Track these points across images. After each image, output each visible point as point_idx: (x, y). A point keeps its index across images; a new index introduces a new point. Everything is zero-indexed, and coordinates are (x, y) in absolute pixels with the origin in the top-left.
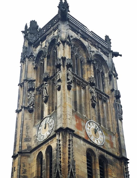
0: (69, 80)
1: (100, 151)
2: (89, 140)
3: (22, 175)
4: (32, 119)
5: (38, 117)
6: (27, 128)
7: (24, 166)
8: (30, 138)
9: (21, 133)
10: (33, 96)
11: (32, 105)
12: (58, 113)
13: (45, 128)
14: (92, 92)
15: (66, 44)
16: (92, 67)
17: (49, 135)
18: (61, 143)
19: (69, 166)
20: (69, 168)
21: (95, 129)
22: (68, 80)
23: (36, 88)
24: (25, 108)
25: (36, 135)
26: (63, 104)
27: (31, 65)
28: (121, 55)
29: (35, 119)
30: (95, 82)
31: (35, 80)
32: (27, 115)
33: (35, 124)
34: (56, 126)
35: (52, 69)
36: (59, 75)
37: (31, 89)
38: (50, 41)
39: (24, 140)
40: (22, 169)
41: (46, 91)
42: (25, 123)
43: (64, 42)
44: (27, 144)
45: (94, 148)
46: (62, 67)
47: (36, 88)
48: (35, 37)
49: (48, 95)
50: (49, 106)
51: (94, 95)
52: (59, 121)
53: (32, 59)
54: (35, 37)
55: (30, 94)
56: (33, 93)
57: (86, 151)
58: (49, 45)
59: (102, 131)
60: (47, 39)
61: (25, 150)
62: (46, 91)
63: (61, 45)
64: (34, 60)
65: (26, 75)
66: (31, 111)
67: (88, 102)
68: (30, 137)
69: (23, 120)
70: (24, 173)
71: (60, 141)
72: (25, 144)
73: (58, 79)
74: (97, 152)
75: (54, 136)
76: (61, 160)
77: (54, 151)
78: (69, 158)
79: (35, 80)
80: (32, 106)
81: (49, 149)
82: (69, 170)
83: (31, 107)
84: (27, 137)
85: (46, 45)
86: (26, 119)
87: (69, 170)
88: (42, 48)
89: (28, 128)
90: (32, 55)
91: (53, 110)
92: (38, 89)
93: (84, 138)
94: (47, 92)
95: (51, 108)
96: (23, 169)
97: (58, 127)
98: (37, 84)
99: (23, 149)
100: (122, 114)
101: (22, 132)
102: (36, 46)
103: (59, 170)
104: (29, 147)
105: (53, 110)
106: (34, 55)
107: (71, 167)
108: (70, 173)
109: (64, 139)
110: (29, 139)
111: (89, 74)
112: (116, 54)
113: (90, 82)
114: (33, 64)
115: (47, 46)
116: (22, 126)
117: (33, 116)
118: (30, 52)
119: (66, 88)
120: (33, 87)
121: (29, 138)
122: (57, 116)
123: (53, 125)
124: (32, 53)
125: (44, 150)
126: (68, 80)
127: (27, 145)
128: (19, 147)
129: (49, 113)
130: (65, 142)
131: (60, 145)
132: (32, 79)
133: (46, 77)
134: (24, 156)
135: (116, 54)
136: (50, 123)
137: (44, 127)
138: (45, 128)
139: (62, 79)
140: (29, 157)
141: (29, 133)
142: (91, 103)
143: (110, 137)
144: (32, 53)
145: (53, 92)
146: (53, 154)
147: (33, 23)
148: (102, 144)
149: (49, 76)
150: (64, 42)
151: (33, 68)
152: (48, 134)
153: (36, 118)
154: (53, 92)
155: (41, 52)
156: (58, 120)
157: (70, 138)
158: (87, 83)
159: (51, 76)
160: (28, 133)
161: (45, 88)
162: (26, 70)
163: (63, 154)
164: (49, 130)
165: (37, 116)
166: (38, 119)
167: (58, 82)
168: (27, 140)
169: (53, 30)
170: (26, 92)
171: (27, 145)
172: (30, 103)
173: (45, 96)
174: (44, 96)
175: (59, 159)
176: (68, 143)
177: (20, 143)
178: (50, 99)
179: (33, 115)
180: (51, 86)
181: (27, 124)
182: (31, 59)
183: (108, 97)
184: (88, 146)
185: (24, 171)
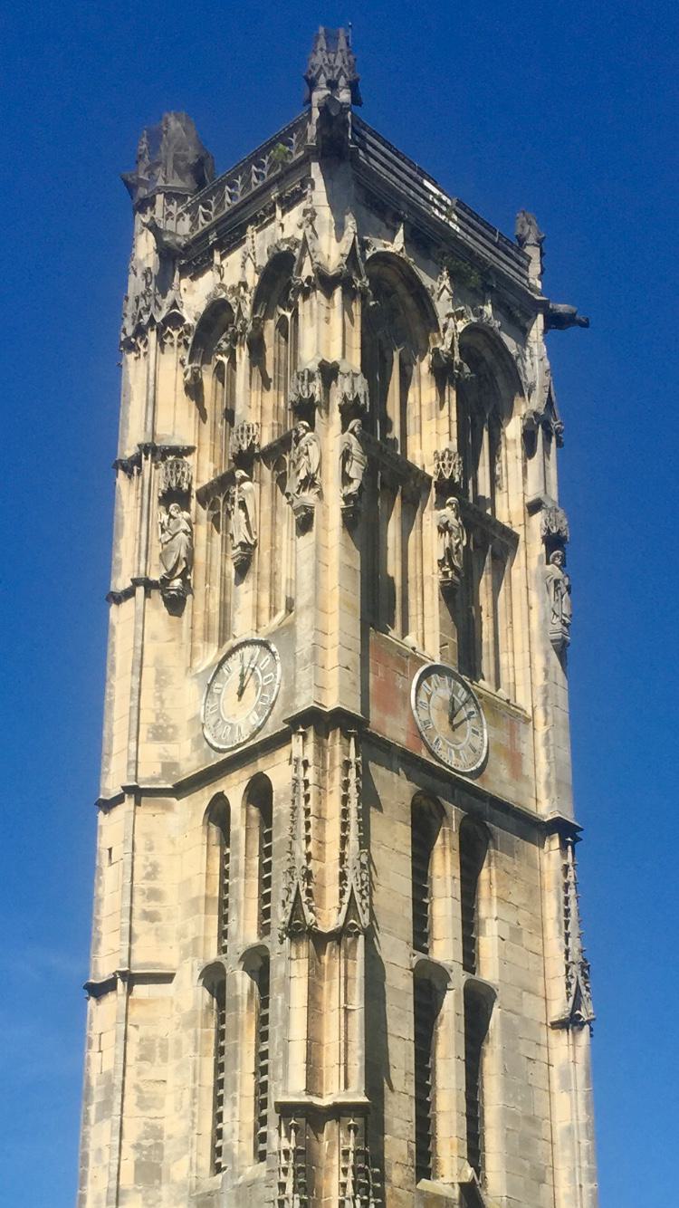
0: (351, 480)
2: (424, 754)
4: (181, 636)
5: (207, 629)
6: (162, 680)
7: (151, 849)
8: (173, 727)
9: (136, 702)
10: (185, 532)
12: (298, 638)
13: (240, 694)
17: (259, 729)
18: (311, 775)
21: (452, 701)
23: (195, 487)
24: (149, 585)
29: (192, 636)
31: (189, 451)
33: (196, 664)
34: (291, 694)
35: (269, 406)
36: (307, 454)
38: (263, 261)
39: (149, 732)
41: (247, 516)
42: (148, 660)
43: (326, 282)
44: (162, 751)
47: (195, 487)
48: (187, 217)
49: (255, 537)
52: (304, 677)
53: (176, 334)
54: (187, 217)
55: (171, 517)
56: (186, 514)
57: (409, 803)
58: (261, 281)
59: (478, 708)
60: (249, 241)
61: (154, 780)
62: (247, 516)
64: (185, 342)
65: (150, 418)
67: (427, 572)
68: (172, 722)
69: (139, 643)
70: (149, 876)
71: (306, 764)
73: (302, 475)
75: (280, 740)
76: (311, 804)
77: (283, 800)
79: (189, 451)
80: (178, 577)
81: (260, 793)
82: (342, 893)
84: (161, 721)
85: (243, 275)
86: (154, 638)
88: (222, 286)
89: (165, 681)
90: (175, 319)
91: (273, 611)
92: (206, 497)
93: (404, 751)
94: (248, 524)
96: (147, 859)
97: (303, 703)
98: (202, 470)
99: (144, 773)
101: (139, 695)
102: (195, 271)
103: (303, 894)
105: (273, 611)
106: (185, 315)
108: (345, 908)
109: (324, 760)
110: (170, 730)
113: (441, 475)
114: (182, 362)
115: (251, 285)
116: (138, 669)
117: (185, 625)
120: (185, 486)
121: (168, 726)
122: (298, 649)
123: (277, 686)
124: (174, 305)
125: (234, 788)
127: (160, 756)
128: (129, 763)
129: (258, 625)
130: (322, 772)
131: (306, 783)
132: (176, 442)
133: (245, 447)
137: (236, 689)
138: (240, 694)
141: (167, 704)
143: (512, 734)
144: (174, 305)
145: (274, 524)
146: (274, 815)
147: (381, 810)
148: (473, 764)
149: (259, 445)
150: (326, 282)
151: (181, 387)
152: (256, 720)
153: (199, 634)
154: (274, 524)
155: (218, 313)
156: (300, 672)
157: (348, 755)
159: (266, 440)
160: (162, 702)
161: (243, 505)
162: (151, 394)
163: (318, 823)
164: (257, 707)
165: (199, 624)
166: (207, 638)
167: (304, 490)
169: (279, 199)
170: (155, 501)
171: (160, 756)
172: (170, 567)
173: (241, 544)
174: (236, 542)
175: (304, 842)
177: (133, 744)
178: (262, 557)
180: (332, 999)
181: (158, 661)
182: (172, 336)
185: (149, 869)
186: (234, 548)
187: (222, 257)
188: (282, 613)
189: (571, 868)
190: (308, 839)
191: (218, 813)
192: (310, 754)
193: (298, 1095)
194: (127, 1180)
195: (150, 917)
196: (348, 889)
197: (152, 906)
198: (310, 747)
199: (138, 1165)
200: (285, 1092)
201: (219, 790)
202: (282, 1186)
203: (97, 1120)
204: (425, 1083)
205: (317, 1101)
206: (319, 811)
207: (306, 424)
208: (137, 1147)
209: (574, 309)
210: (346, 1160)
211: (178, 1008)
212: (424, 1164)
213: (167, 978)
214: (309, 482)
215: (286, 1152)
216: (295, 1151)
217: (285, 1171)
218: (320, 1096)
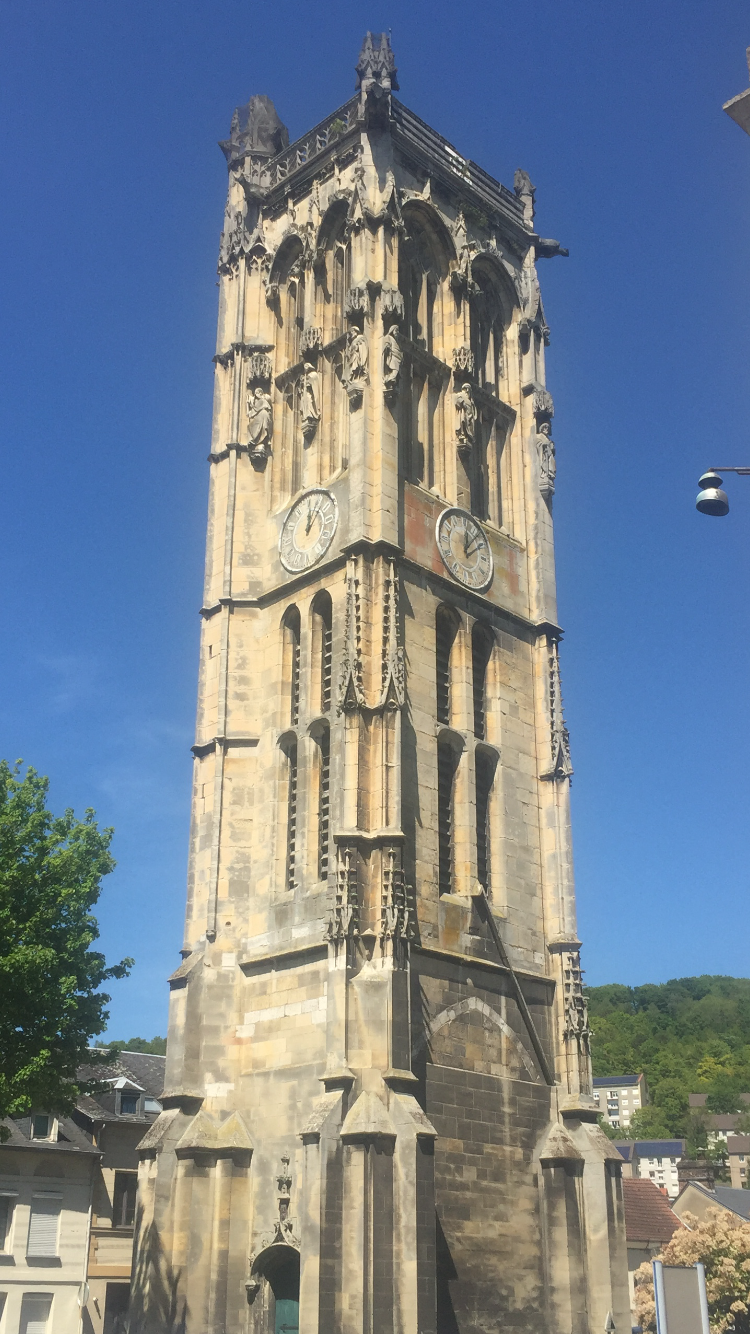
10: (267, 409)
18: (361, 591)
24: (240, 449)
25: (276, 547)
31: (270, 349)
41: (313, 398)
81: (322, 604)
82: (384, 679)
130: (369, 589)
186: (303, 421)
190: (358, 639)
191: (292, 620)
192: (360, 575)
194: (223, 894)
195: (241, 697)
197: (242, 689)
199: (232, 883)
200: (342, 828)
202: (339, 898)
205: (365, 835)
207: (357, 328)
212: (446, 882)
213: (253, 743)
215: (342, 873)
217: (342, 887)
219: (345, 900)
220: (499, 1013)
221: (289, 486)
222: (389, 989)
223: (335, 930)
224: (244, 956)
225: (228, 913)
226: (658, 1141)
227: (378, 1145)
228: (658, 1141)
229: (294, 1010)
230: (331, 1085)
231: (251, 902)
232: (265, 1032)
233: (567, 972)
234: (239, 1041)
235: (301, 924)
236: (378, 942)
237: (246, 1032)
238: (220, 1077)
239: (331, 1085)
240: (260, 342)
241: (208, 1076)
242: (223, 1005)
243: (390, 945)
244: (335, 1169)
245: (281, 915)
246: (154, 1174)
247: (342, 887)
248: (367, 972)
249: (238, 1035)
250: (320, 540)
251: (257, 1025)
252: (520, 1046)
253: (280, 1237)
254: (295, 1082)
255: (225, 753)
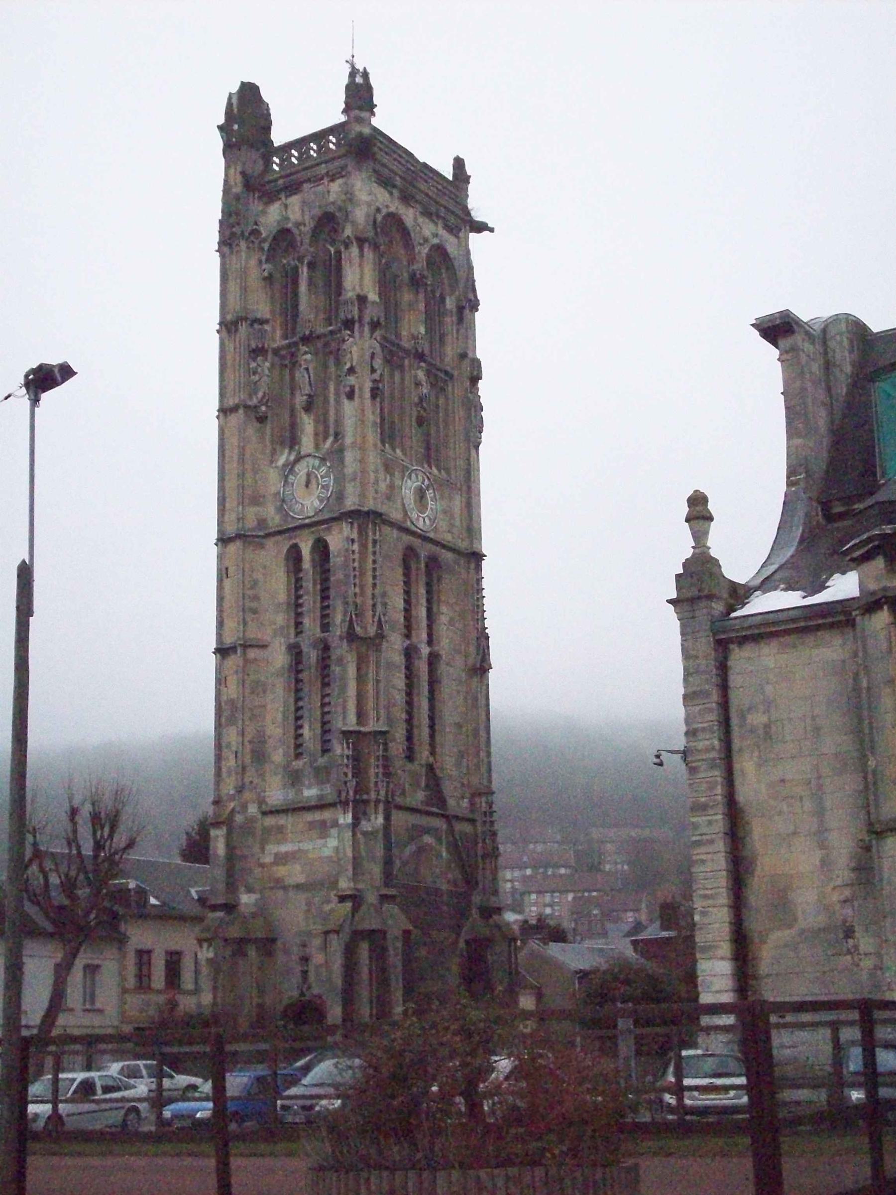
1: (429, 546)
3: (250, 593)
10: (268, 376)
11: (266, 404)
13: (307, 486)
14: (418, 384)
15: (366, 245)
16: (421, 296)
18: (356, 547)
19: (374, 605)
20: (374, 611)
22: (373, 370)
24: (246, 407)
25: (279, 493)
26: (359, 440)
27: (253, 265)
28: (492, 230)
30: (427, 352)
31: (267, 321)
32: (251, 431)
35: (321, 305)
37: (257, 352)
40: (248, 579)
41: (309, 377)
42: (247, 456)
45: (417, 542)
46: (357, 325)
50: (317, 421)
51: (425, 391)
62: (309, 377)
63: (355, 250)
64: (263, 249)
66: (262, 419)
72: (252, 513)
73: (348, 366)
74: (424, 550)
78: (374, 585)
79: (267, 321)
81: (322, 549)
82: (374, 616)
83: (263, 408)
87: (374, 616)
90: (255, 233)
95: (321, 428)
100: (480, 432)
104: (262, 523)
107: (379, 608)
111: (413, 326)
112: (480, 227)
113: (417, 351)
118: (251, 221)
119: (367, 395)
126: (373, 370)
130: (364, 546)
134: (250, 543)
135: (480, 227)
136: (322, 477)
138: (307, 486)
139: (358, 369)
140: (262, 546)
142: (415, 414)
158: (407, 352)
166: (282, 443)
168: (256, 500)
176: (370, 545)
178: (319, 401)
179: (268, 427)
183: (451, 377)
184: (407, 538)
186: (302, 396)
187: (287, 197)
188: (331, 439)
189: (409, 215)
190: (355, 585)
191: (294, 556)
192: (355, 536)
193: (353, 726)
194: (248, 759)
195: (255, 611)
196: (377, 614)
197: (254, 605)
198: (355, 531)
199: (253, 751)
200: (345, 724)
201: (295, 542)
202: (346, 774)
203: (227, 725)
204: (685, 1120)
205: (362, 729)
206: (360, 567)
207: (349, 332)
208: (250, 742)
209: (840, 931)
210: (378, 760)
211: (502, 844)
212: (410, 757)
213: (264, 647)
214: (352, 370)
215: (348, 757)
216: (352, 756)
217: (347, 766)
218: (364, 726)
219: (350, 775)
220: (441, 844)
221: (288, 442)
222: (381, 835)
223: (344, 794)
224: (263, 806)
225: (251, 775)
226: (187, 1049)
227: (376, 937)
228: (187, 1049)
229: (306, 846)
230: (342, 899)
231: (267, 767)
232: (281, 859)
233: (485, 813)
234: (262, 866)
235: (309, 787)
236: (372, 804)
237: (268, 859)
238: (250, 890)
239: (342, 899)
240: (259, 316)
241: (242, 889)
242: (250, 840)
243: (381, 807)
244: (350, 952)
245: (294, 779)
246: (211, 955)
247: (347, 766)
248: (365, 826)
249: (261, 861)
250: (318, 497)
251: (276, 855)
252: (453, 865)
253: (302, 994)
254: (310, 895)
255: (244, 653)
